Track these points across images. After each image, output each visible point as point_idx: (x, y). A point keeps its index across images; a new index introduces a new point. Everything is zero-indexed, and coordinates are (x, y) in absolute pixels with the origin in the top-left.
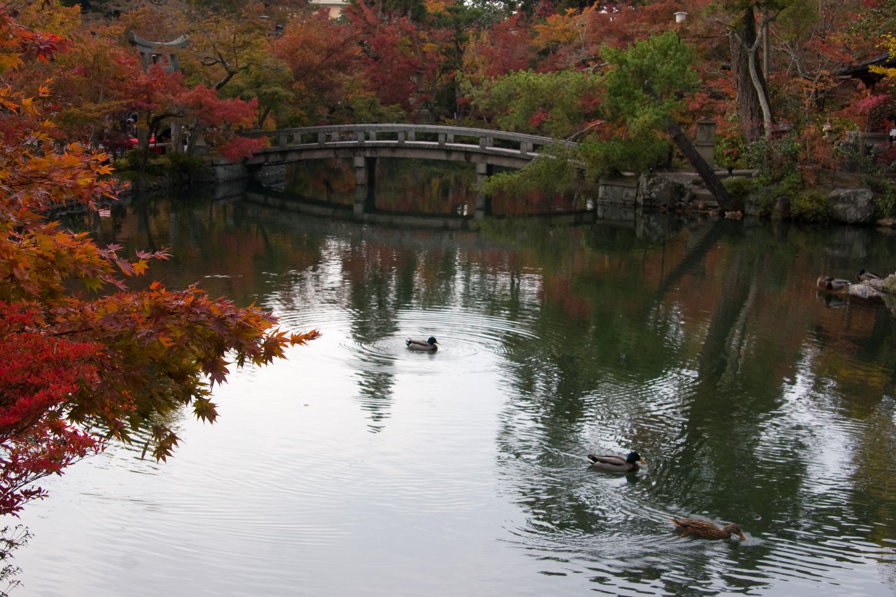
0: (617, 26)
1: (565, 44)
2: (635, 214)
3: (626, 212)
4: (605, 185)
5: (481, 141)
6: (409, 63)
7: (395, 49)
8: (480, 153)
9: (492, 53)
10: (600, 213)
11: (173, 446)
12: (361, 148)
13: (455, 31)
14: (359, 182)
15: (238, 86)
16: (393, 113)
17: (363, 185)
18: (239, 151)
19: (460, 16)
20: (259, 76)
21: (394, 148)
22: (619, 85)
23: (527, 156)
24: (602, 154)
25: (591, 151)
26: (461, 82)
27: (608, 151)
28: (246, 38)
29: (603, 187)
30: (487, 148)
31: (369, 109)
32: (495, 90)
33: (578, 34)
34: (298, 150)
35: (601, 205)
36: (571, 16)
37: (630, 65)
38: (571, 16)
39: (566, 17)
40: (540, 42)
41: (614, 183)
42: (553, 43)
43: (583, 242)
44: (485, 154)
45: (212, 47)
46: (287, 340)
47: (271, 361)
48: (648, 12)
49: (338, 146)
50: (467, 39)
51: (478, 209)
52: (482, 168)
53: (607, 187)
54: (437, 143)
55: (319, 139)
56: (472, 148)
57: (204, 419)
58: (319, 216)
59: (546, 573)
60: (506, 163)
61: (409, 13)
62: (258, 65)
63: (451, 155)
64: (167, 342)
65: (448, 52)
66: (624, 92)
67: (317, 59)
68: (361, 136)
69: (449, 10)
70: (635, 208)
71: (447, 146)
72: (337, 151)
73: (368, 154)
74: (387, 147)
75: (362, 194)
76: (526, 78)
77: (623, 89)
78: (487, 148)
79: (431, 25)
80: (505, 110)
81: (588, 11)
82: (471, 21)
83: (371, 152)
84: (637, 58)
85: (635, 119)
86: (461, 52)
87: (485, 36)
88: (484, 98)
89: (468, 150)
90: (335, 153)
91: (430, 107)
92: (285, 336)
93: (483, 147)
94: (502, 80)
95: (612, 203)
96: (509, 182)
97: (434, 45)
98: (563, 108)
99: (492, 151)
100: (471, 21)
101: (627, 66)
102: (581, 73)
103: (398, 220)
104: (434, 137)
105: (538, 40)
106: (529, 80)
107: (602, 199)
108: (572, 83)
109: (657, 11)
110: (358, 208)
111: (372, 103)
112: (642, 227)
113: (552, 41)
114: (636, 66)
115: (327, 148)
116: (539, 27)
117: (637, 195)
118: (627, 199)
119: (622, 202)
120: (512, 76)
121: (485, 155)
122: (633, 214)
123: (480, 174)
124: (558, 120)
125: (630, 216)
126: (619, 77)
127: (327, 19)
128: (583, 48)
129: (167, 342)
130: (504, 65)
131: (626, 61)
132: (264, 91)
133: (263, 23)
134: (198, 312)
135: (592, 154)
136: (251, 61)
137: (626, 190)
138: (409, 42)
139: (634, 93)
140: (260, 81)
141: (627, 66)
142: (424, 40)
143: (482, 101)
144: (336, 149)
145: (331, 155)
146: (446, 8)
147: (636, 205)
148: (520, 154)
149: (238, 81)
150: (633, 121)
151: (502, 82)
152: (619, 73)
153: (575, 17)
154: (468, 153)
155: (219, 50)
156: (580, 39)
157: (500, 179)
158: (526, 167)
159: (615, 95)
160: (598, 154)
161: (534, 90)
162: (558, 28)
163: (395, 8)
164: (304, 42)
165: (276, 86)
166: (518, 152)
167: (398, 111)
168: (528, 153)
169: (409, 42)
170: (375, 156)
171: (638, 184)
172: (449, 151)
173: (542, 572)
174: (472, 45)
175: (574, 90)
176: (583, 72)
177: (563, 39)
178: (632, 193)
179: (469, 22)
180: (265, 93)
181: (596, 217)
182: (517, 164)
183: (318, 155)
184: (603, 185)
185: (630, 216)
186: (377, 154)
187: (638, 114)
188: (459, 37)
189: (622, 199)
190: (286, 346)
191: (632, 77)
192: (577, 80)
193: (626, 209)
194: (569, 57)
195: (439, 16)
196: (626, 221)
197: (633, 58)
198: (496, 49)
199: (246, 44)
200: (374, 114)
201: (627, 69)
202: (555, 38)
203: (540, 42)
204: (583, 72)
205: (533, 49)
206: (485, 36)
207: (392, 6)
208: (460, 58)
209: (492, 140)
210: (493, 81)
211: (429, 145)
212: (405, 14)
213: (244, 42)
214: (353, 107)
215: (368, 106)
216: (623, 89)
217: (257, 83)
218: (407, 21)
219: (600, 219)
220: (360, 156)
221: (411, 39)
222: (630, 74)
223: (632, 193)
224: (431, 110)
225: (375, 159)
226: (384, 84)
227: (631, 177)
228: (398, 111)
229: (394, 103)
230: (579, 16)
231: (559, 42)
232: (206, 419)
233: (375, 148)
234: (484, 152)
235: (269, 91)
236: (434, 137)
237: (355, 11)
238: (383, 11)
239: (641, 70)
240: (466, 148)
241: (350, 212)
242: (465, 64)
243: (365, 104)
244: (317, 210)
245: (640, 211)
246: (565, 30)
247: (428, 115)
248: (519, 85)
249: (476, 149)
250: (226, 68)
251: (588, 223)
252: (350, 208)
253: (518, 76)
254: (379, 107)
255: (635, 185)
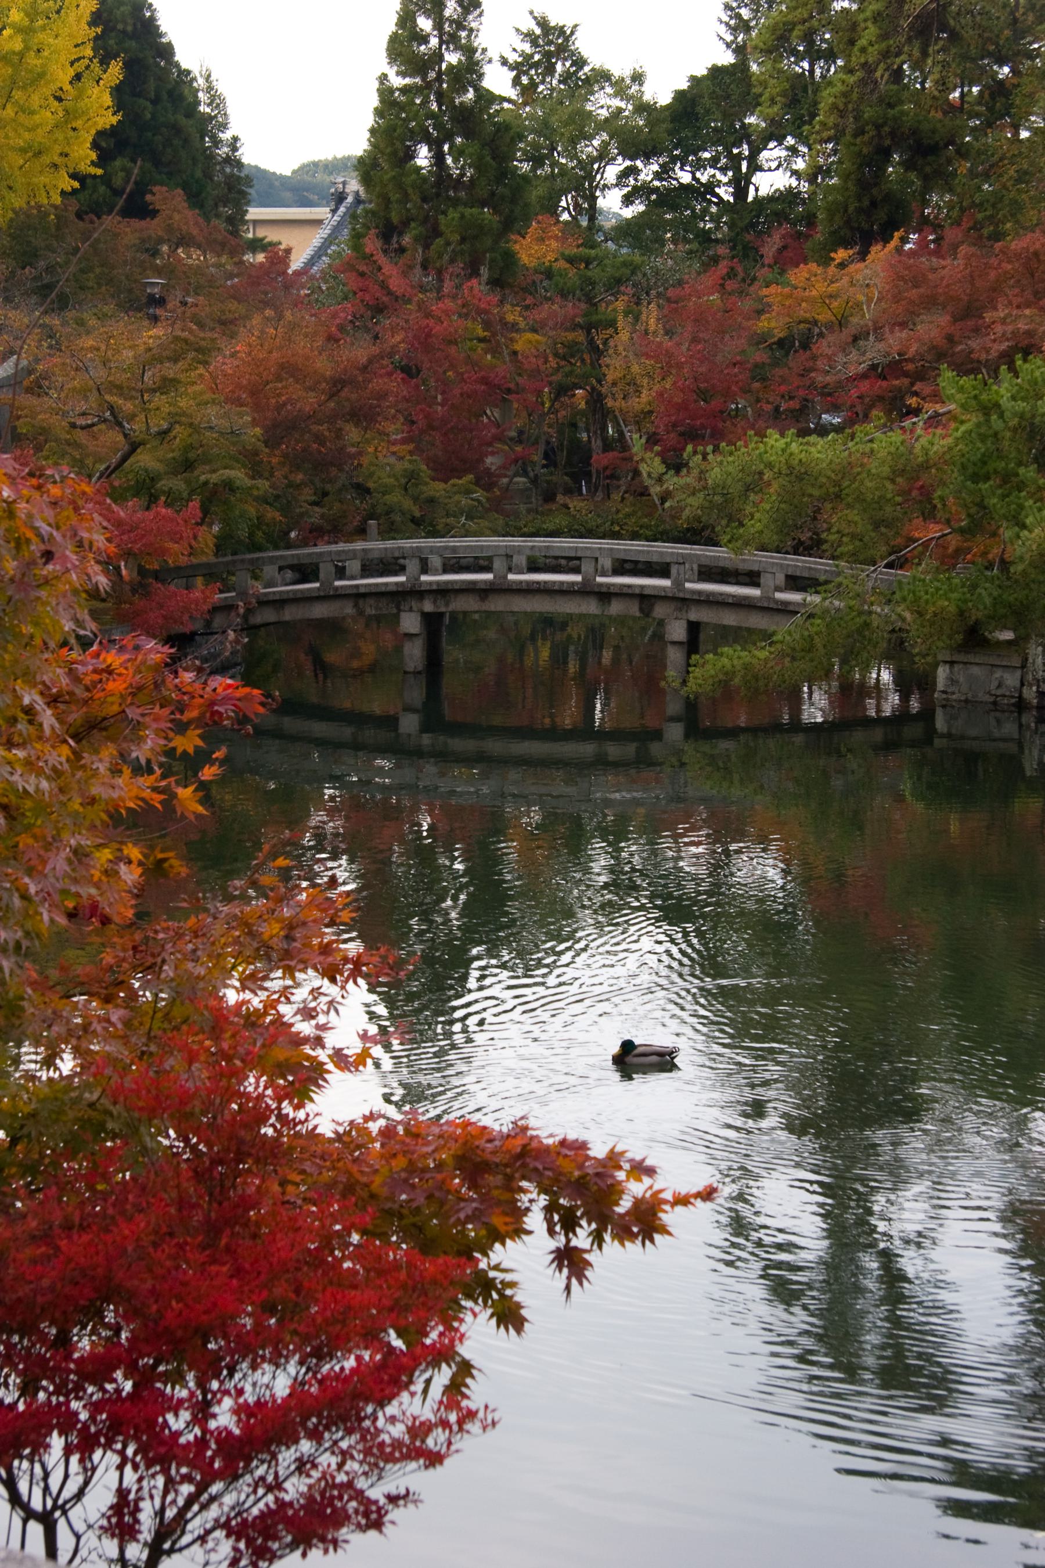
0: (948, 286)
1: (830, 326)
2: (1021, 726)
3: (998, 721)
4: (952, 663)
5: (674, 570)
6: (484, 380)
7: (452, 350)
8: (674, 599)
9: (669, 354)
10: (940, 723)
11: (469, 1381)
12: (415, 592)
13: (583, 306)
14: (410, 666)
15: (146, 471)
16: (457, 497)
17: (419, 673)
18: (164, 617)
19: (594, 272)
20: (191, 447)
21: (483, 592)
22: (984, 455)
23: (776, 601)
24: (952, 609)
25: (927, 602)
26: (642, 460)
27: (965, 601)
28: (171, 370)
29: (947, 667)
30: (688, 585)
31: (406, 489)
32: (715, 475)
33: (859, 305)
34: (275, 602)
35: (944, 706)
36: (842, 265)
37: (1007, 414)
38: (842, 265)
39: (832, 269)
40: (773, 324)
41: (971, 658)
42: (802, 326)
43: (906, 787)
44: (684, 600)
45: (95, 392)
46: (666, 1202)
47: (652, 1241)
48: (1018, 256)
49: (362, 590)
50: (612, 324)
51: (673, 719)
52: (677, 631)
53: (956, 667)
54: (578, 578)
55: (322, 575)
56: (654, 587)
57: (507, 1330)
58: (321, 743)
59: (976, 1542)
60: (730, 619)
61: (484, 271)
62: (191, 425)
63: (609, 602)
64: (506, 1224)
65: (570, 351)
66: (996, 472)
67: (309, 401)
68: (412, 566)
69: (571, 260)
70: (1020, 713)
71: (601, 585)
72: (361, 602)
73: (428, 607)
74: (470, 589)
75: (416, 694)
76: (783, 450)
77: (991, 466)
78: (688, 585)
79: (529, 289)
80: (736, 519)
81: (879, 253)
82: (619, 281)
83: (435, 602)
84: (1023, 399)
85: (1025, 533)
86: (598, 352)
87: (652, 316)
88: (694, 494)
89: (646, 592)
90: (356, 605)
91: (532, 474)
92: (663, 1196)
93: (678, 584)
94: (731, 454)
95: (967, 701)
96: (747, 667)
97: (537, 337)
98: (865, 510)
99: (700, 593)
100: (619, 281)
101: (1001, 416)
102: (899, 431)
103: (495, 746)
104: (570, 563)
105: (769, 320)
106: (791, 454)
107: (944, 692)
108: (882, 454)
109: (1036, 254)
110: (409, 723)
111: (412, 476)
112: (1036, 753)
113: (800, 322)
114: (1022, 416)
115: (339, 596)
116: (773, 293)
117: (1022, 684)
118: (999, 692)
119: (992, 699)
120: (752, 445)
121: (683, 601)
122: (1016, 727)
123: (674, 643)
124: (853, 536)
125: (1009, 728)
126: (983, 438)
127: (285, 273)
128: (871, 338)
129: (506, 1224)
130: (696, 379)
131: (997, 405)
132: (203, 478)
133: (204, 339)
134: (540, 1167)
135: (932, 609)
136: (175, 419)
137: (998, 674)
138: (480, 332)
139: (1017, 475)
140: (192, 455)
141: (1001, 416)
142: (514, 327)
143: (690, 500)
144: (358, 596)
145: (349, 609)
146: (563, 254)
147: (1021, 705)
148: (761, 598)
149: (145, 460)
150: (1018, 537)
151: (730, 459)
152: (983, 430)
153: (852, 267)
154: (646, 599)
155: (108, 397)
156: (863, 316)
157: (725, 661)
158: (784, 629)
159: (976, 478)
160: (943, 609)
161: (800, 478)
162: (814, 293)
163: (452, 261)
164: (281, 367)
165: (231, 468)
166: (755, 592)
167: (468, 492)
168: (779, 595)
169: (480, 332)
170: (443, 609)
171: (1026, 659)
172: (605, 595)
173: (984, 1543)
174: (624, 336)
175: (886, 470)
176: (902, 428)
177: (824, 316)
178: (1011, 680)
179: (615, 284)
180: (206, 483)
181: (931, 732)
182: (756, 621)
183: (320, 611)
184: (946, 662)
185: (1009, 728)
186: (447, 605)
187: (1029, 521)
188: (595, 318)
189: (989, 693)
190: (666, 1212)
191: (1012, 440)
192: (893, 449)
193: (998, 714)
194: (841, 358)
195: (549, 274)
196: (1004, 740)
197: (1014, 398)
198: (678, 344)
199: (166, 385)
200: (415, 499)
201: (1000, 422)
202: (808, 315)
203: (773, 324)
204: (902, 428)
205: (759, 340)
206: (652, 316)
207: (446, 257)
208: (596, 365)
209: (695, 567)
210: (710, 457)
211: (562, 583)
212: (475, 273)
213: (164, 379)
214: (371, 485)
215: (403, 481)
216: (991, 466)
217: (187, 460)
218: (478, 287)
219: (942, 736)
220: (411, 610)
221: (487, 325)
222: (1008, 434)
223: (1011, 680)
224: (535, 481)
225: (441, 615)
226: (431, 427)
227: (1009, 643)
228: (468, 492)
229: (460, 474)
230: (861, 265)
231: (815, 323)
232: (510, 1327)
233: (443, 592)
234: (681, 595)
235: (214, 478)
236: (570, 563)
237: (363, 268)
238: (425, 266)
239: (1032, 424)
240: (642, 587)
241: (393, 734)
242: (610, 378)
243: (397, 479)
244: (320, 728)
245: (1029, 719)
246: (831, 296)
247: (527, 489)
248: (770, 466)
249: (664, 588)
250: (126, 436)
251: (913, 744)
252: (390, 722)
253: (765, 444)
254: (426, 484)
255: (1016, 662)
